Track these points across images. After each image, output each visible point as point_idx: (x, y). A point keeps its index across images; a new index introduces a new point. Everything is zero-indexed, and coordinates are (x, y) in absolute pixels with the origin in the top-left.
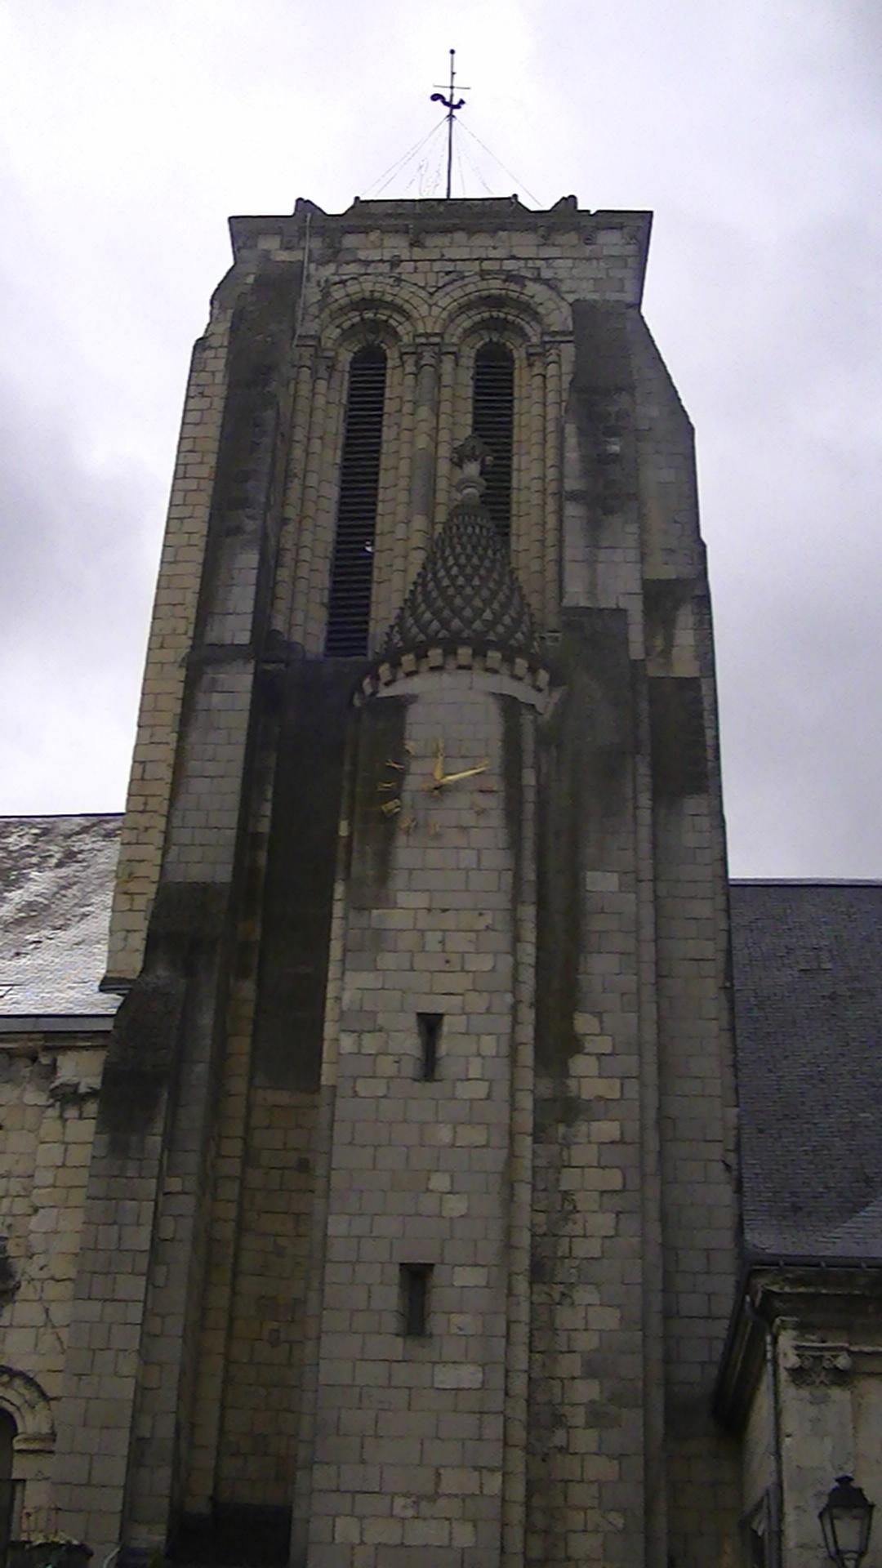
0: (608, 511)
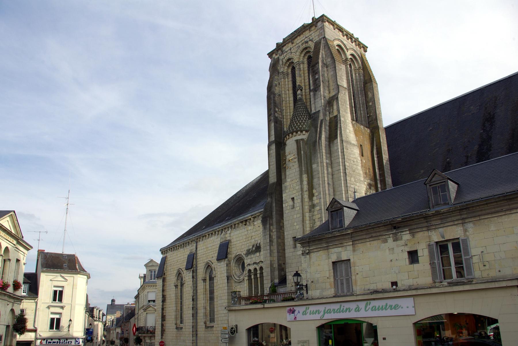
0: (316, 91)
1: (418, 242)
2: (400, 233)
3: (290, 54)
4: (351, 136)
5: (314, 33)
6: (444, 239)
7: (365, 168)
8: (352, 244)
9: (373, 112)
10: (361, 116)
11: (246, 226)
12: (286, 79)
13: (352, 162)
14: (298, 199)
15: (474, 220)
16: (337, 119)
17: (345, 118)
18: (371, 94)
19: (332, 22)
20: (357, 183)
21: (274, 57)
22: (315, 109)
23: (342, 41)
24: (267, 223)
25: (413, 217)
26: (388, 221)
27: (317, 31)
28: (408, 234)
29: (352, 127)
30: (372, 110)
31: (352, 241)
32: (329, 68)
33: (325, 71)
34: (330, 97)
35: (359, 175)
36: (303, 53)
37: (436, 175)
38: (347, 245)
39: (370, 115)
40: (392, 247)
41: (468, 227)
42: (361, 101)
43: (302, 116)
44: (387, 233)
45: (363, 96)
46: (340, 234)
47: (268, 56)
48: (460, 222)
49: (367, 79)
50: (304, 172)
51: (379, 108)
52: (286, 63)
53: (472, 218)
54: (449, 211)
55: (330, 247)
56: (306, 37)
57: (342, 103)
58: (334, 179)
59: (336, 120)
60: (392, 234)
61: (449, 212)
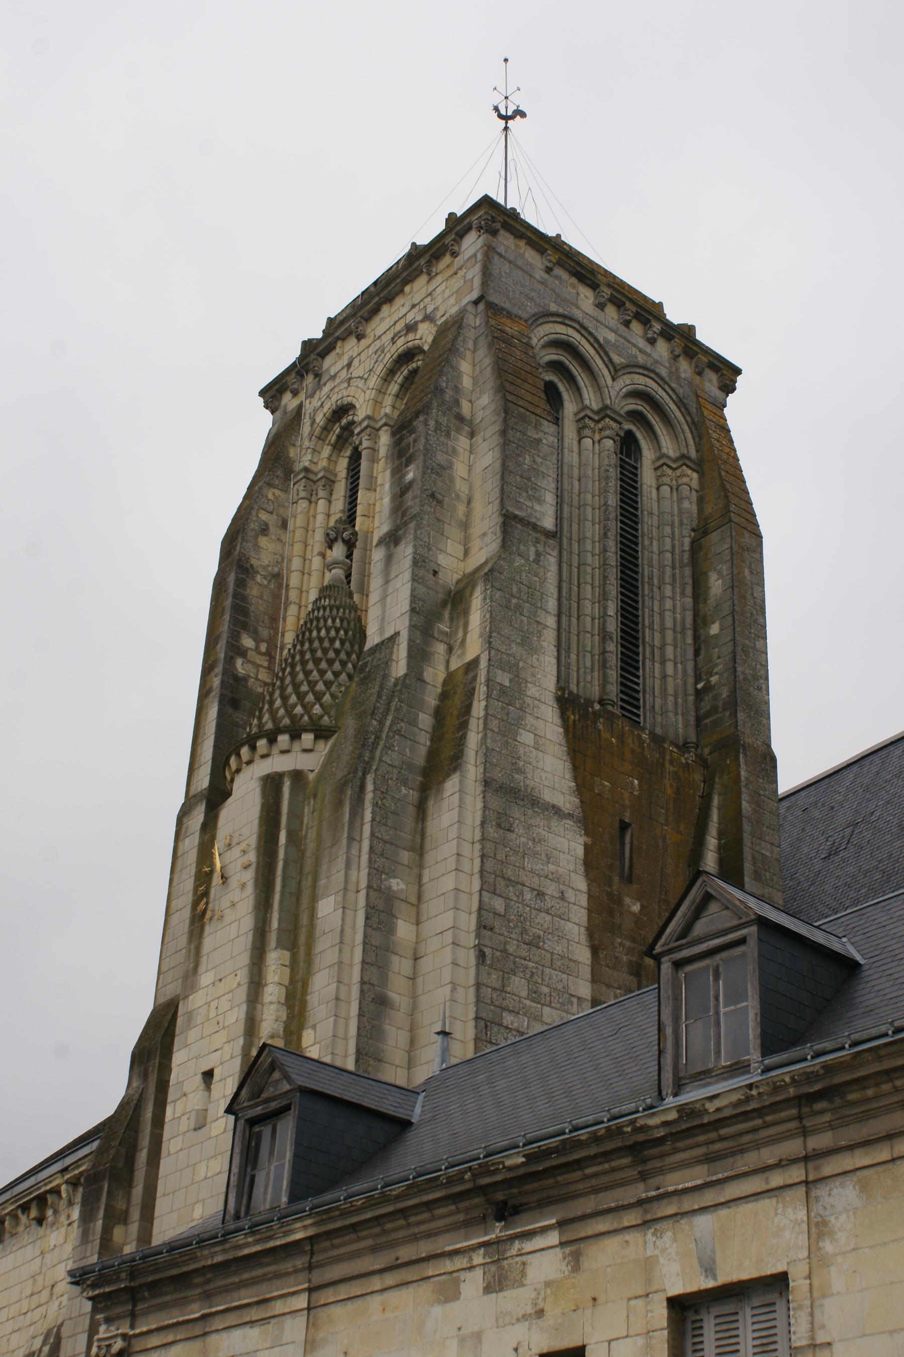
1: (594, 1299)
2: (517, 1245)
3: (346, 385)
4: (540, 765)
5: (444, 284)
6: (715, 1277)
7: (633, 940)
8: (309, 1309)
9: (720, 667)
10: (664, 689)
11: (41, 1231)
12: (322, 505)
13: (528, 896)
14: (225, 1079)
15: (866, 1161)
16: (475, 678)
17: (517, 676)
18: (720, 581)
19: (533, 237)
20: (546, 1010)
21: (286, 406)
22: (382, 629)
23: (586, 329)
24: (99, 1208)
25: (577, 1144)
26: (465, 1172)
27: (456, 274)
28: (553, 1250)
29: (558, 721)
30: (719, 657)
31: (306, 1285)
32: (478, 439)
33: (461, 450)
34: (464, 574)
35: (568, 965)
36: (395, 379)
37: (713, 907)
38: (284, 1314)
39: (708, 682)
40: (476, 1329)
41: (832, 1206)
42: (668, 615)
43: (331, 662)
44: (466, 1239)
45: (683, 594)
46: (258, 1248)
47: (261, 400)
48: (796, 1174)
49: (710, 511)
50: (273, 938)
51: (755, 648)
52: (326, 429)
53: (857, 1152)
54: (743, 1109)
55: (218, 1323)
56: (413, 306)
57: (514, 601)
58: (420, 980)
59: (470, 683)
60: (482, 1251)
61: (745, 1116)
